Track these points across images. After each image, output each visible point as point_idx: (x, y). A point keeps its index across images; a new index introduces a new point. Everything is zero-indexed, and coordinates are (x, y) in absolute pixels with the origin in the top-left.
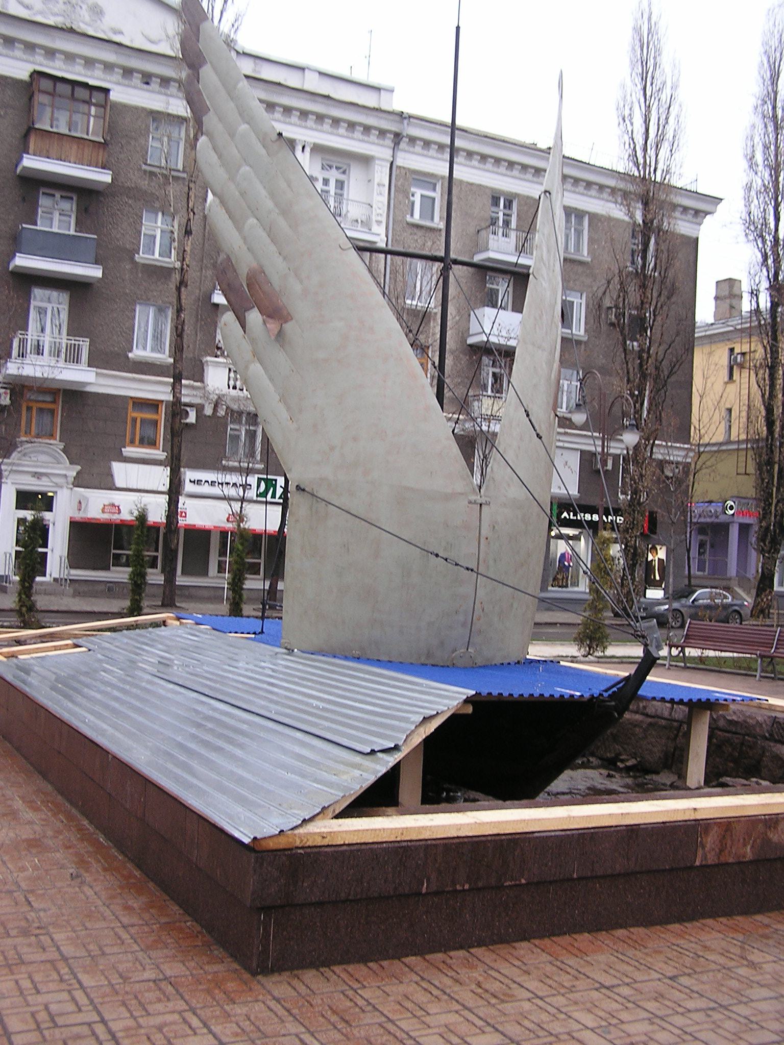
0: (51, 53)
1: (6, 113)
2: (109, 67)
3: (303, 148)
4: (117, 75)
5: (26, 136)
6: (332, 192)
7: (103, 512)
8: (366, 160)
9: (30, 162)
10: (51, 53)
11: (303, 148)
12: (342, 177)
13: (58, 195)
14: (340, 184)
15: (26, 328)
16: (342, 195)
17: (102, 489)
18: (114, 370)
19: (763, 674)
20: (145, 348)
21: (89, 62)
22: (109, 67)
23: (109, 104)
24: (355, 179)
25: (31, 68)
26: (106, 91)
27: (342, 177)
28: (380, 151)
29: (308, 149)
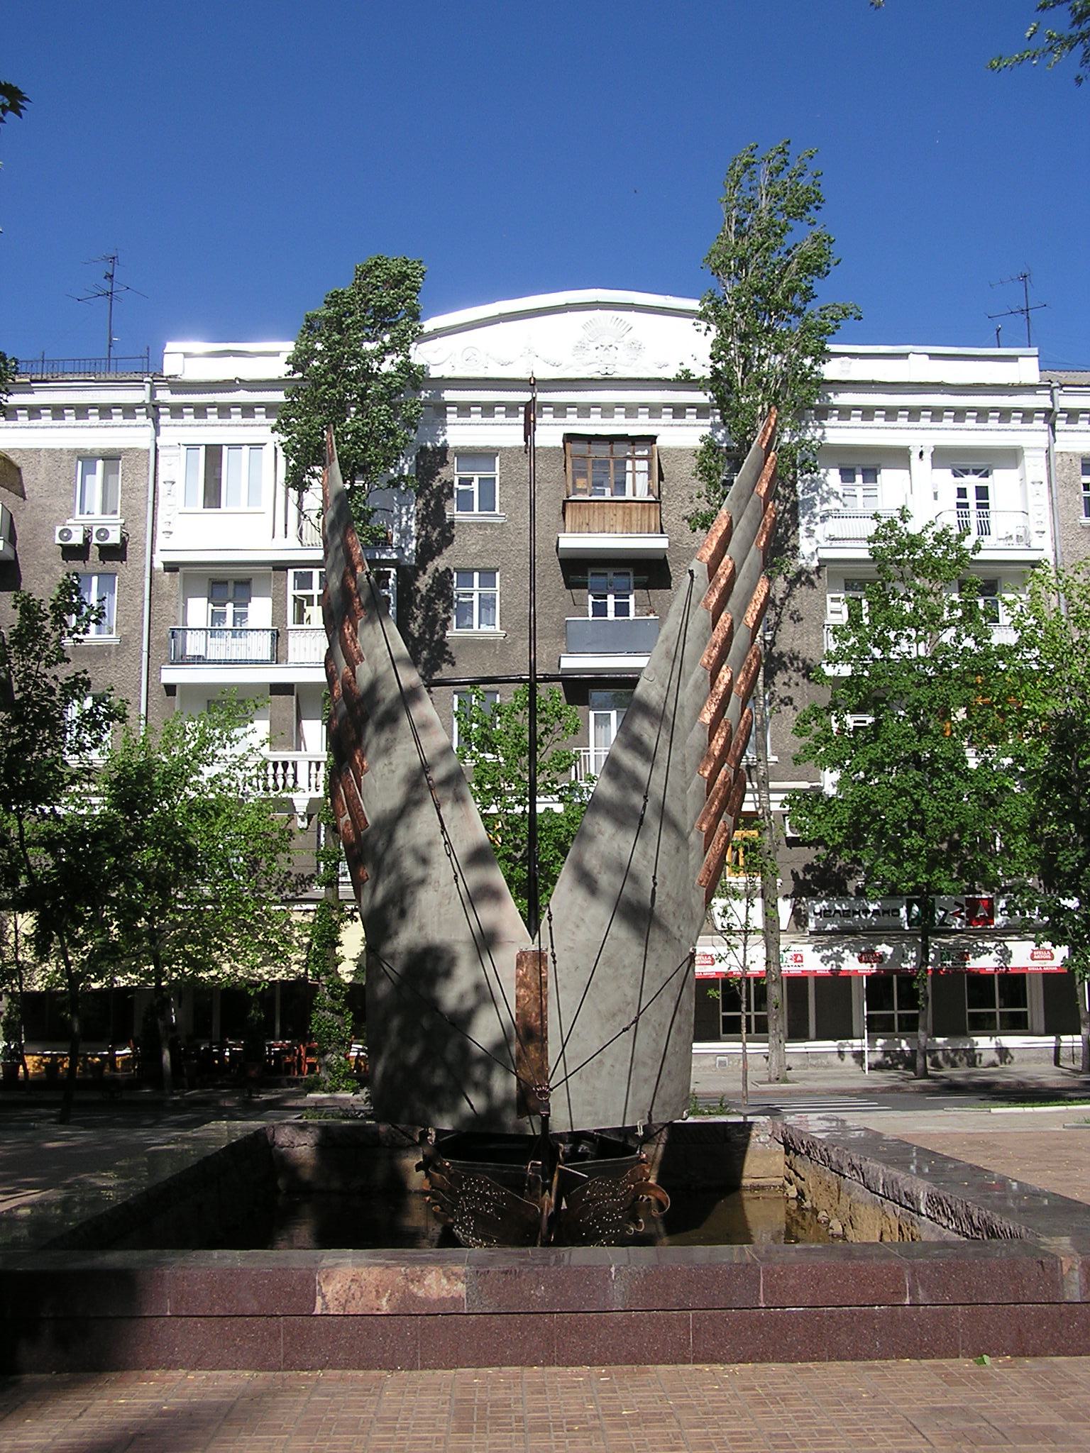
0: (584, 410)
2: (655, 410)
3: (921, 454)
6: (973, 506)
8: (1012, 457)
11: (921, 454)
12: (983, 482)
14: (982, 492)
15: (493, 1113)
16: (987, 506)
22: (655, 410)
24: (1001, 482)
26: (652, 439)
27: (983, 482)
28: (1032, 437)
29: (927, 456)
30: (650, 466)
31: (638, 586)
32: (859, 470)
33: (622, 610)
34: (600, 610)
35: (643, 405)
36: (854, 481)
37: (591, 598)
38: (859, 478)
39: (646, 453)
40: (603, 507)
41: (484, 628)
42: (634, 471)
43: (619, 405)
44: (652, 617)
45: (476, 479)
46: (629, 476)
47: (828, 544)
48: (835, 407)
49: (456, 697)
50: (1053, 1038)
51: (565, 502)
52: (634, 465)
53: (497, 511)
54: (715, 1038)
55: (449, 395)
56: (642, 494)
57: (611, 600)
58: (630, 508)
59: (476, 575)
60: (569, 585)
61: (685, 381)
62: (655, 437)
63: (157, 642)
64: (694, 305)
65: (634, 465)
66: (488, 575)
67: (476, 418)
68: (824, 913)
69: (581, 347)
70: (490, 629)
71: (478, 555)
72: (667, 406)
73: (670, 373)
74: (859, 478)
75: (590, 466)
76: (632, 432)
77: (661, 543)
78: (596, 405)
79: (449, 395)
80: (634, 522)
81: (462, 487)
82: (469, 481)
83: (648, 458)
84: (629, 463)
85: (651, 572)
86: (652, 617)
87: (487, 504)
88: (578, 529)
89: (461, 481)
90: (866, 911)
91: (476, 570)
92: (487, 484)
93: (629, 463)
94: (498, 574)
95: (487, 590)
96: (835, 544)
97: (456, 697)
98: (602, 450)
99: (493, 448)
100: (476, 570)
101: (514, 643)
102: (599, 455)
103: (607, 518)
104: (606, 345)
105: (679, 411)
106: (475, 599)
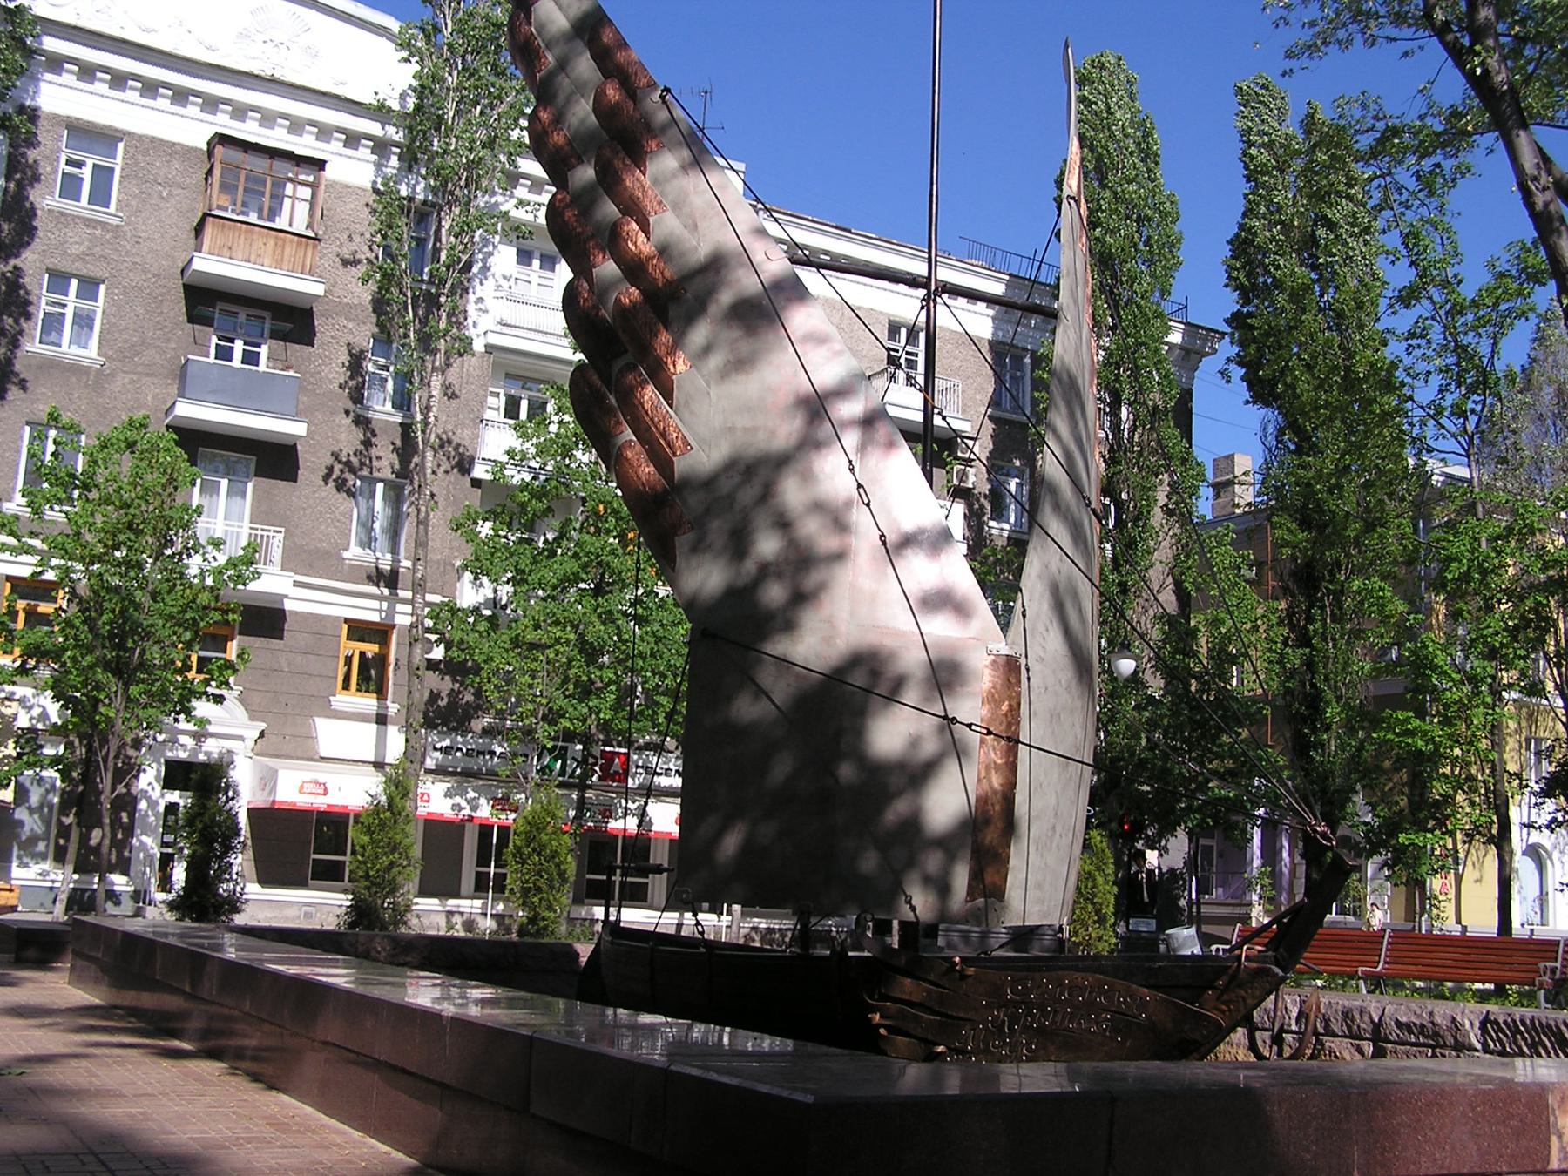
0: (240, 112)
1: (170, 195)
4: (336, 145)
5: (199, 230)
7: (301, 792)
9: (207, 264)
10: (240, 112)
13: (242, 317)
17: (298, 759)
18: (316, 616)
19: (250, 185)
20: (362, 654)
21: (296, 126)
22: (324, 132)
23: (323, 183)
25: (209, 132)
26: (320, 164)
30: (314, 195)
31: (275, 335)
32: (537, 254)
33: (251, 358)
34: (225, 354)
35: (312, 123)
36: (529, 264)
37: (214, 340)
38: (536, 263)
39: (311, 179)
40: (252, 232)
41: (75, 350)
42: (294, 198)
43: (284, 116)
44: (291, 373)
45: (90, 163)
46: (287, 202)
47: (499, 328)
48: (43, 53)
49: (28, 429)
50: (677, 915)
51: (205, 215)
52: (295, 190)
53: (112, 208)
54: (301, 884)
55: (51, 44)
56: (300, 226)
57: (239, 346)
58: (284, 240)
59: (74, 282)
60: (192, 319)
61: (379, 112)
62: (325, 162)
63: (284, 240)
64: (394, 25)
65: (295, 190)
66: (89, 287)
67: (133, 96)
68: (447, 751)
69: (244, 35)
70: (81, 352)
71: (80, 258)
72: (340, 130)
73: (367, 98)
74: (536, 263)
75: (242, 179)
76: (299, 151)
77: (317, 289)
78: (256, 109)
79: (51, 44)
80: (286, 257)
81: (69, 169)
82: (79, 164)
83: (314, 186)
84: (289, 186)
85: (291, 321)
86: (291, 373)
87: (100, 195)
88: (217, 252)
89: (69, 162)
90: (493, 753)
91: (75, 276)
92: (103, 175)
93: (289, 186)
94: (102, 288)
95: (86, 304)
96: (506, 330)
97: (28, 429)
98: (259, 164)
99: (117, 130)
100: (75, 276)
101: (112, 375)
102: (249, 171)
103: (255, 247)
104: (277, 41)
105: (352, 139)
106: (69, 312)
